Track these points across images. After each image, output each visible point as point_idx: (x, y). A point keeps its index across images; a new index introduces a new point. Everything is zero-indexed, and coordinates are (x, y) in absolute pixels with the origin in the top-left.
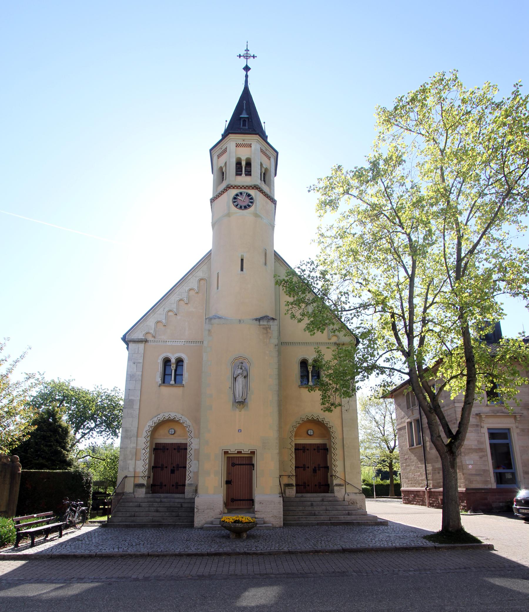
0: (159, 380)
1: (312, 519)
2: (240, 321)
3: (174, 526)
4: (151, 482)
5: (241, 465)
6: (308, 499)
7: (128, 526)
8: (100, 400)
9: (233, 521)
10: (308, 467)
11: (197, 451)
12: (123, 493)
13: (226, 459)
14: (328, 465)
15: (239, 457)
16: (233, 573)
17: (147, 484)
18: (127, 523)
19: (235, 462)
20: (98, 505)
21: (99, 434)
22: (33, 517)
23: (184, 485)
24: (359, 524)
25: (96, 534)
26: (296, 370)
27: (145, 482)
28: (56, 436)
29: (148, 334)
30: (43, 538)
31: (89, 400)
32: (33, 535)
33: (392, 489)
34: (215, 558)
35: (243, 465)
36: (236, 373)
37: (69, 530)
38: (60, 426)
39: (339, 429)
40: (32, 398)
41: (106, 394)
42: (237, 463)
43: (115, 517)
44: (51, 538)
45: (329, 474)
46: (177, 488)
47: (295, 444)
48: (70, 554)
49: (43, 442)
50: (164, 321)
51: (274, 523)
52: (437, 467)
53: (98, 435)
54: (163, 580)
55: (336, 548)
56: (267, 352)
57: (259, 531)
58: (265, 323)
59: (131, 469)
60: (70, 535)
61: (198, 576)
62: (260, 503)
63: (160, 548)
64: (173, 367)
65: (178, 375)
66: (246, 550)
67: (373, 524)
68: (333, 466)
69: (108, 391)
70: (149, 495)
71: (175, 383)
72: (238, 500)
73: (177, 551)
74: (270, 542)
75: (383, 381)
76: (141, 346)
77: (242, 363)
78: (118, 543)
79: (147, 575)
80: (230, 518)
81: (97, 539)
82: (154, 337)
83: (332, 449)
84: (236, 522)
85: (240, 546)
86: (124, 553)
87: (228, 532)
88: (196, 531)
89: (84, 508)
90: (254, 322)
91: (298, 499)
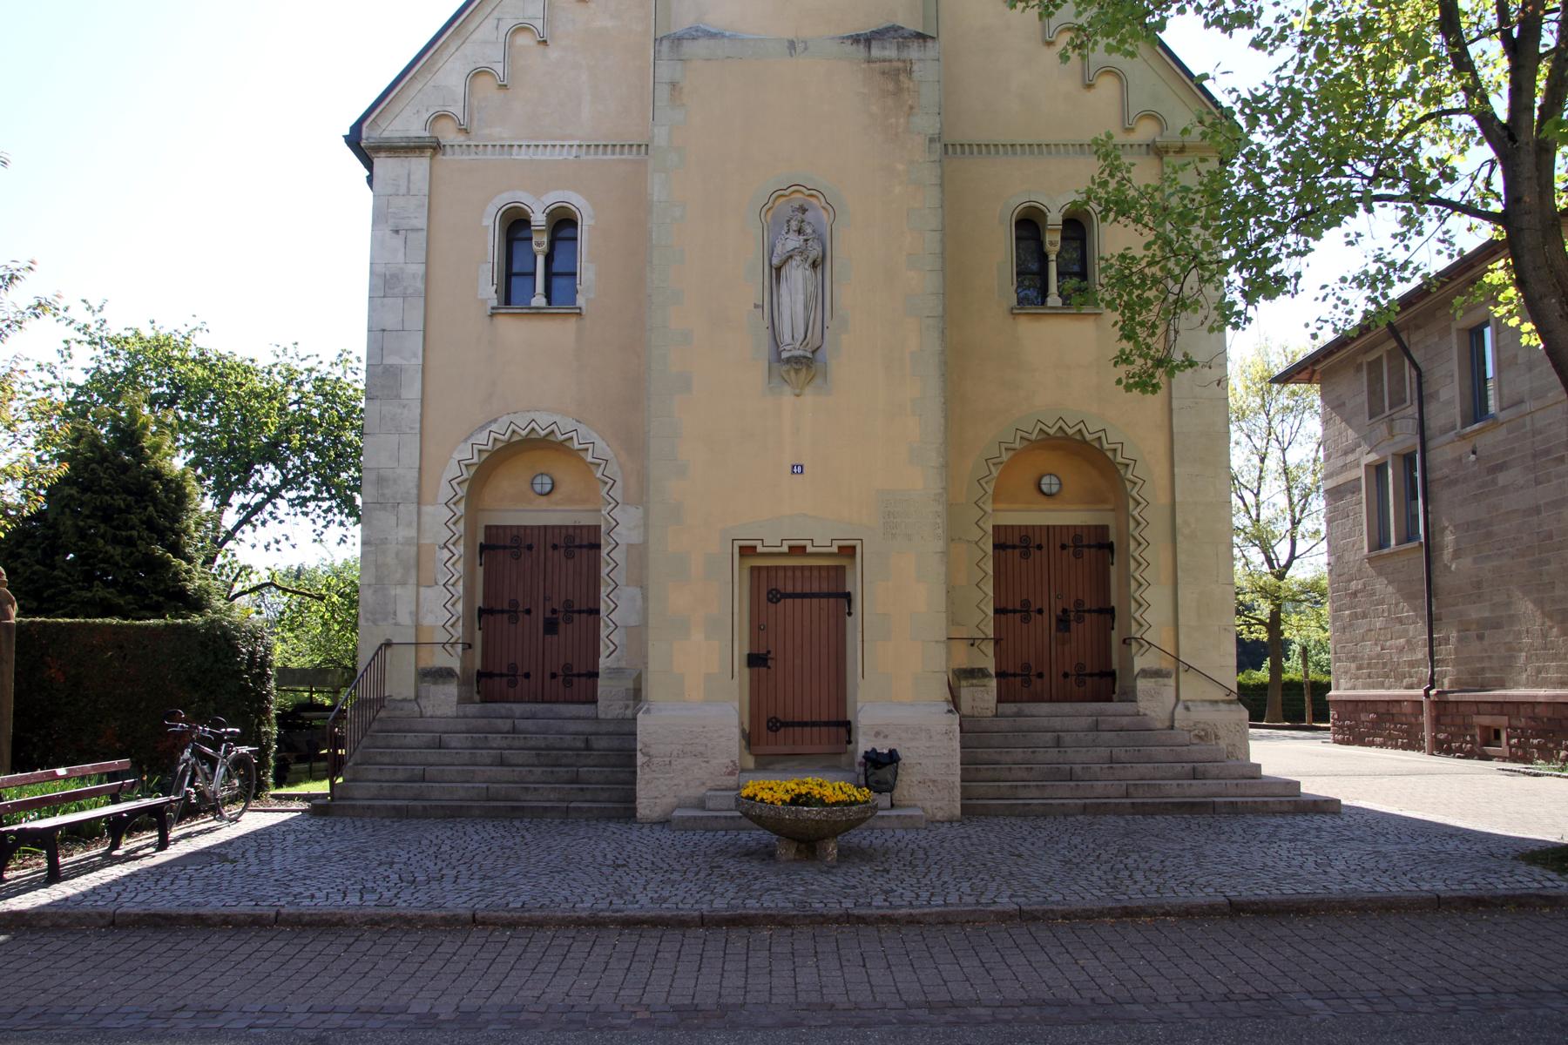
0: (489, 292)
1: (1062, 793)
2: (792, 45)
3: (566, 814)
4: (478, 665)
5: (803, 596)
6: (1044, 722)
7: (401, 814)
8: (294, 397)
9: (787, 798)
10: (1040, 611)
11: (640, 553)
12: (380, 702)
13: (746, 574)
14: (1114, 603)
15: (794, 568)
16: (814, 998)
17: (463, 669)
18: (398, 803)
19: (780, 587)
20: (305, 743)
21: (298, 509)
22: (55, 777)
23: (594, 675)
24: (1235, 810)
25: (291, 838)
26: (1000, 250)
27: (455, 664)
28: (145, 508)
29: (444, 123)
30: (101, 850)
31: (257, 396)
32: (47, 841)
33: (1276, 698)
34: (733, 936)
35: (812, 595)
36: (778, 250)
37: (199, 824)
38: (157, 474)
39: (1160, 470)
40: (72, 391)
41: (314, 374)
42: (789, 589)
43: (354, 780)
44: (128, 852)
45: (1115, 635)
46: (568, 683)
47: (996, 528)
48: (182, 911)
49: (102, 528)
50: (499, 68)
51: (928, 804)
52: (1474, 616)
53: (292, 511)
54: (536, 1025)
55: (1199, 897)
56: (900, 167)
57: (877, 833)
58: (891, 52)
59: (405, 618)
60: (195, 838)
61: (676, 1009)
62: (877, 734)
63: (518, 896)
64: (540, 243)
65: (560, 277)
66: (848, 904)
67: (1285, 808)
68: (1133, 605)
69: (320, 367)
70: (472, 709)
71: (549, 302)
72: (793, 724)
73: (584, 909)
74: (933, 875)
75: (1378, 259)
76: (419, 166)
77: (804, 210)
78: (361, 874)
79: (470, 1003)
80: (775, 788)
81: (290, 857)
82: (466, 131)
83: (1133, 545)
84: (797, 800)
85: (823, 889)
86: (382, 911)
87: (766, 836)
88: (646, 831)
89: (245, 749)
90: (849, 48)
91: (1004, 724)
